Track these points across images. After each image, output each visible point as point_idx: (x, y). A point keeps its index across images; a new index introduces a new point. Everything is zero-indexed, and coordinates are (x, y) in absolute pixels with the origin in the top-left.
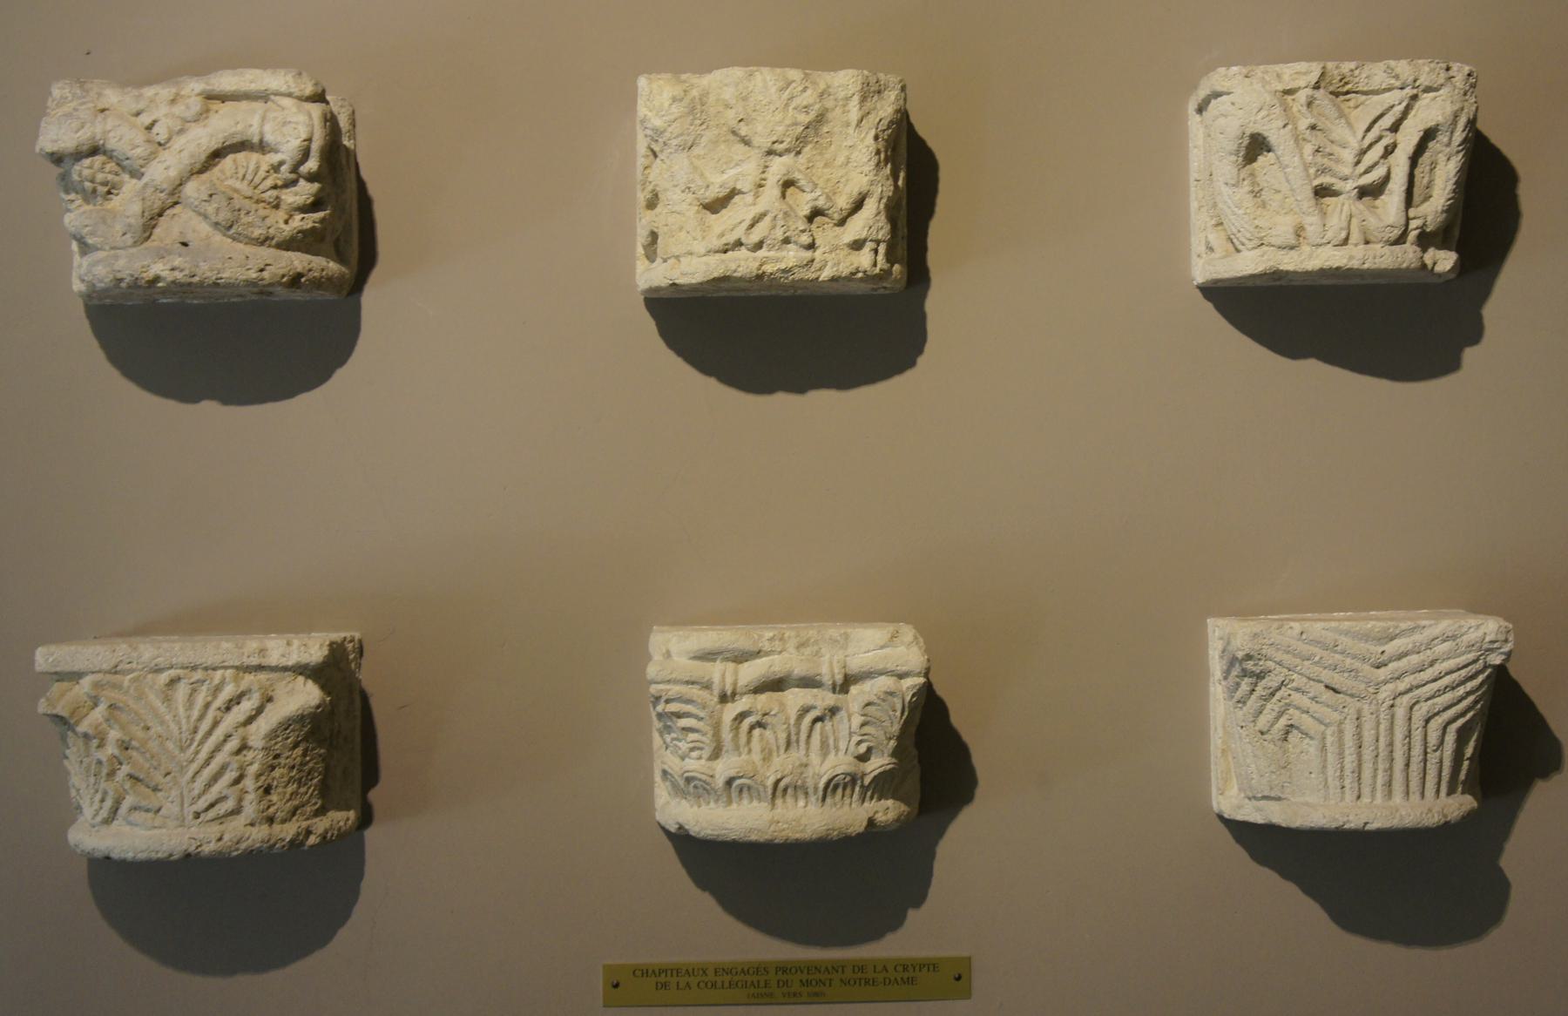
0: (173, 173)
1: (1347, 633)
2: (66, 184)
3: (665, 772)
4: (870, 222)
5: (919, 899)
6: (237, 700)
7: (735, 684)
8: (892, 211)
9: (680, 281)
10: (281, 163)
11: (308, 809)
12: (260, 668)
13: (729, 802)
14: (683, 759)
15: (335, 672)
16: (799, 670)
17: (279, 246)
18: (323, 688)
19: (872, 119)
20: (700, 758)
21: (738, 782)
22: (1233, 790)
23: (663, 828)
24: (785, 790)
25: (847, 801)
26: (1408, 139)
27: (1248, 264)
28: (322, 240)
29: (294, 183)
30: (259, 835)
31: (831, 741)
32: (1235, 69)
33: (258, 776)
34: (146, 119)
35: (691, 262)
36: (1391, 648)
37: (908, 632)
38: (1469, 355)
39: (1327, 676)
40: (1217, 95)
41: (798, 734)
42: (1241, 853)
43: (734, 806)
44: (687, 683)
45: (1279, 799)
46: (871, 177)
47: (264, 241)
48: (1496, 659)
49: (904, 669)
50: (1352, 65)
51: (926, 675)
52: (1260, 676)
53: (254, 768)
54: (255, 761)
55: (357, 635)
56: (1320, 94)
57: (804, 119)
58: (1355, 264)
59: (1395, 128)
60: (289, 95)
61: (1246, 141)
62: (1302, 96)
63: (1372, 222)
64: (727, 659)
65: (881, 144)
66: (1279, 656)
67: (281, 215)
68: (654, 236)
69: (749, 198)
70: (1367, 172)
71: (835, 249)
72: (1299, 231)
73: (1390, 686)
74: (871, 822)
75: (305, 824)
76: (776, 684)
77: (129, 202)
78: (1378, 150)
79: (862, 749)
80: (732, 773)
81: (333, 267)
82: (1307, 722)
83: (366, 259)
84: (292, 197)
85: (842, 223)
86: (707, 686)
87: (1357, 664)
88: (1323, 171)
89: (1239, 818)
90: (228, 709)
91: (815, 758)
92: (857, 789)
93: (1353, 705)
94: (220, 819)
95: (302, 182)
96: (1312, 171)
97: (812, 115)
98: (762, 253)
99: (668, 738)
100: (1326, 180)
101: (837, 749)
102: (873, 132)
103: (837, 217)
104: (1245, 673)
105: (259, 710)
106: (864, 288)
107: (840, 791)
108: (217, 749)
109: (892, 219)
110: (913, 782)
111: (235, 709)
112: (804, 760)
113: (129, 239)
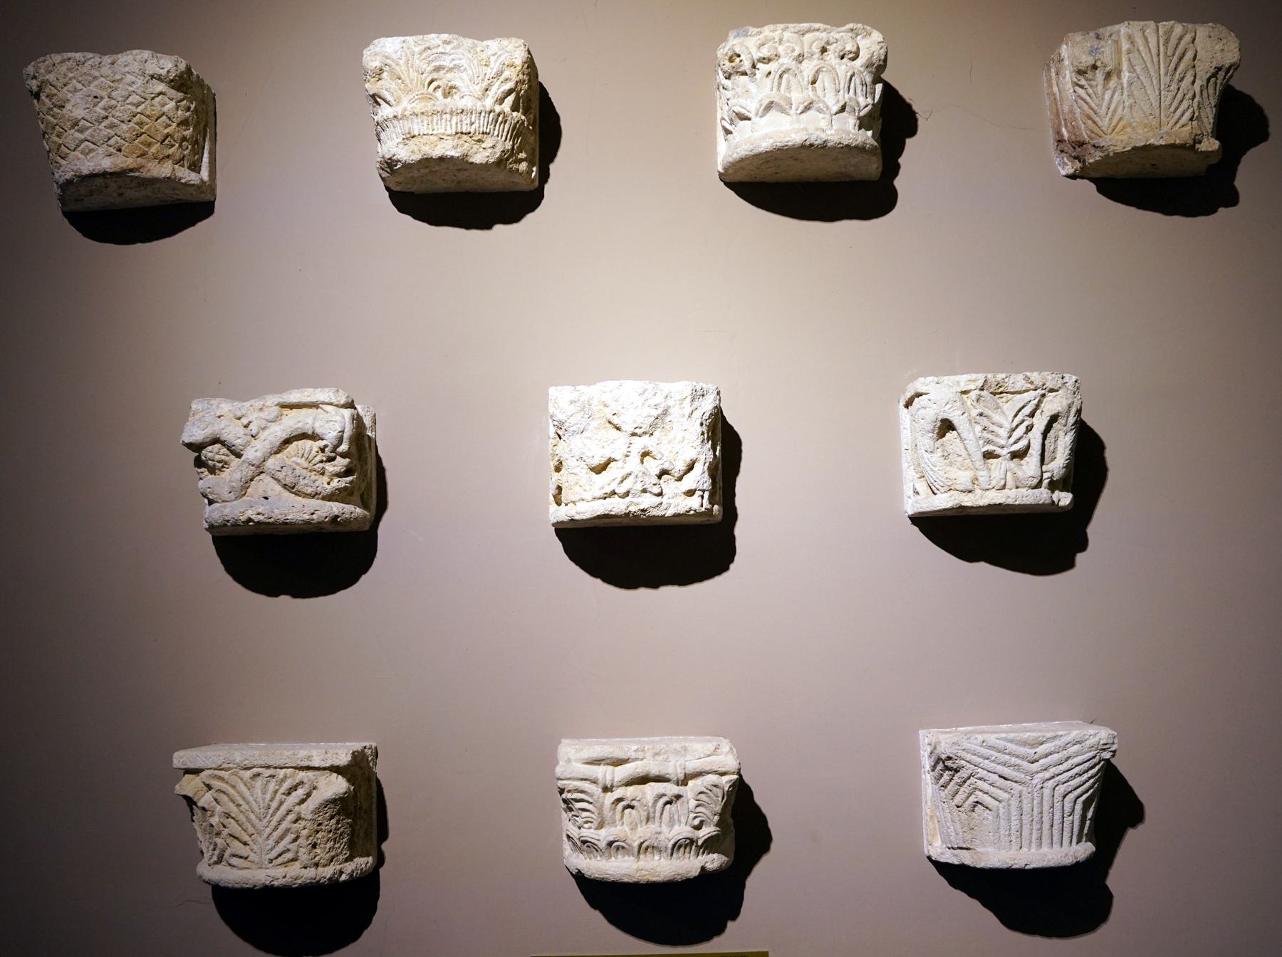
0: (259, 454)
1: (1011, 741)
2: (199, 463)
3: (568, 836)
4: (699, 478)
5: (735, 915)
6: (295, 788)
8: (712, 471)
9: (577, 517)
10: (326, 446)
11: (341, 857)
12: (309, 768)
13: (610, 857)
15: (359, 770)
16: (654, 771)
17: (323, 499)
18: (349, 781)
19: (698, 414)
22: (938, 843)
24: (647, 848)
25: (687, 855)
26: (1040, 422)
27: (943, 502)
28: (351, 494)
29: (333, 459)
30: (310, 874)
32: (930, 379)
33: (308, 838)
34: (245, 421)
35: (587, 501)
36: (1042, 749)
37: (726, 746)
38: (1080, 558)
39: (1000, 769)
40: (919, 395)
42: (943, 882)
45: (968, 849)
46: (698, 449)
47: (313, 496)
48: (1107, 755)
50: (1004, 376)
51: (739, 773)
52: (957, 771)
53: (305, 832)
54: (305, 828)
55: (374, 744)
56: (985, 393)
57: (656, 413)
58: (1010, 501)
59: (1032, 415)
60: (331, 404)
61: (939, 424)
62: (973, 395)
63: (1020, 474)
65: (705, 429)
66: (969, 757)
67: (325, 479)
68: (559, 488)
69: (619, 464)
70: (1015, 443)
71: (676, 495)
72: (975, 480)
73: (1040, 775)
75: (338, 867)
76: (644, 780)
77: (235, 472)
78: (1022, 428)
79: (696, 822)
80: (611, 839)
81: (359, 511)
82: (987, 800)
83: (382, 506)
84: (330, 468)
85: (680, 479)
86: (594, 782)
87: (1019, 761)
88: (989, 442)
89: (942, 860)
90: (289, 794)
91: (665, 829)
93: (1017, 787)
94: (284, 864)
95: (338, 458)
96: (981, 442)
97: (660, 411)
98: (628, 499)
100: (990, 448)
102: (699, 421)
103: (677, 475)
104: (947, 768)
105: (308, 795)
106: (699, 520)
108: (283, 819)
109: (713, 476)
110: (730, 842)
111: (294, 794)
113: (232, 496)
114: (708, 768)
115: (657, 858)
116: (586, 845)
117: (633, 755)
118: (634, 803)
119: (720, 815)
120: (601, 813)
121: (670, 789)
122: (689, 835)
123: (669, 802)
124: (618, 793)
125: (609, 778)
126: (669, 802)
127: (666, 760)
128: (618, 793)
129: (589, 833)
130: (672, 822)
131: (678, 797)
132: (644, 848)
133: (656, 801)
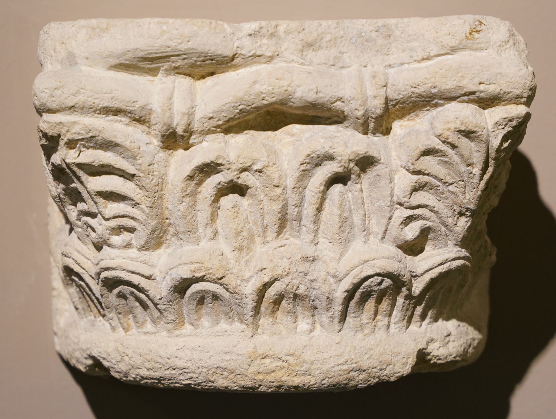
3: (68, 272)
7: (191, 114)
13: (179, 322)
14: (99, 248)
20: (128, 246)
21: (195, 288)
23: (67, 364)
24: (278, 301)
25: (382, 320)
31: (357, 219)
37: (497, 29)
41: (300, 205)
43: (188, 328)
44: (107, 111)
49: (492, 89)
64: (177, 71)
74: (422, 356)
76: (271, 117)
79: (411, 232)
80: (185, 273)
86: (140, 120)
91: (326, 249)
92: (400, 301)
99: (73, 212)
101: (366, 230)
107: (370, 304)
110: (479, 298)
112: (310, 252)
114: (448, 84)
115: (303, 325)
116: (116, 292)
117: (247, 47)
118: (246, 179)
119: (474, 214)
120: (156, 205)
121: (345, 142)
122: (392, 267)
123: (340, 179)
124: (205, 150)
125: (179, 107)
126: (340, 179)
127: (336, 63)
128: (205, 150)
129: (122, 258)
130: (345, 233)
131: (366, 163)
132: (271, 299)
133: (305, 174)
